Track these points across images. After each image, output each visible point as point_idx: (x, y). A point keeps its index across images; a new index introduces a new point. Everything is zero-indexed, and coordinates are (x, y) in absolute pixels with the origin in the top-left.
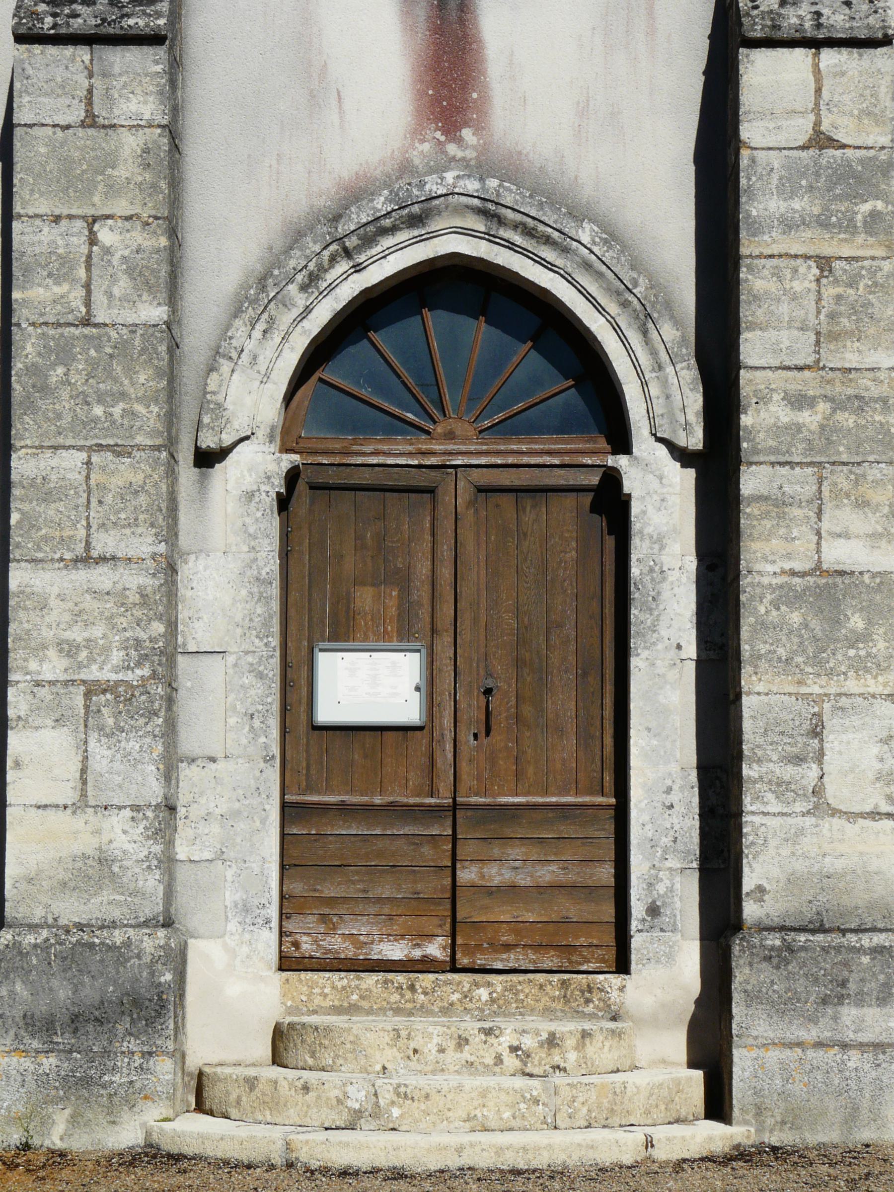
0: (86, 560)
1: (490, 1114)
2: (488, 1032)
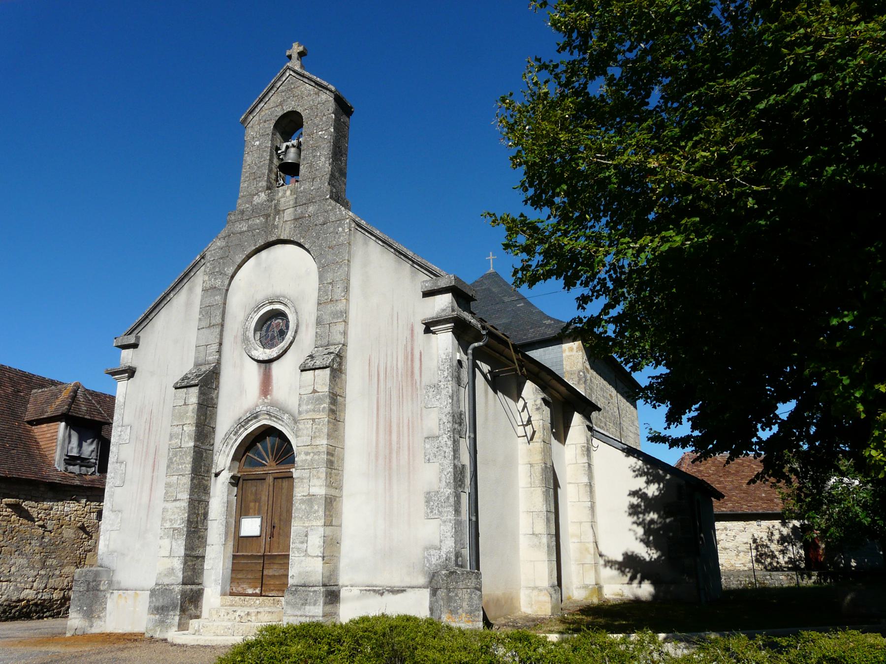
0: (175, 500)
1: (218, 632)
2: (234, 611)
